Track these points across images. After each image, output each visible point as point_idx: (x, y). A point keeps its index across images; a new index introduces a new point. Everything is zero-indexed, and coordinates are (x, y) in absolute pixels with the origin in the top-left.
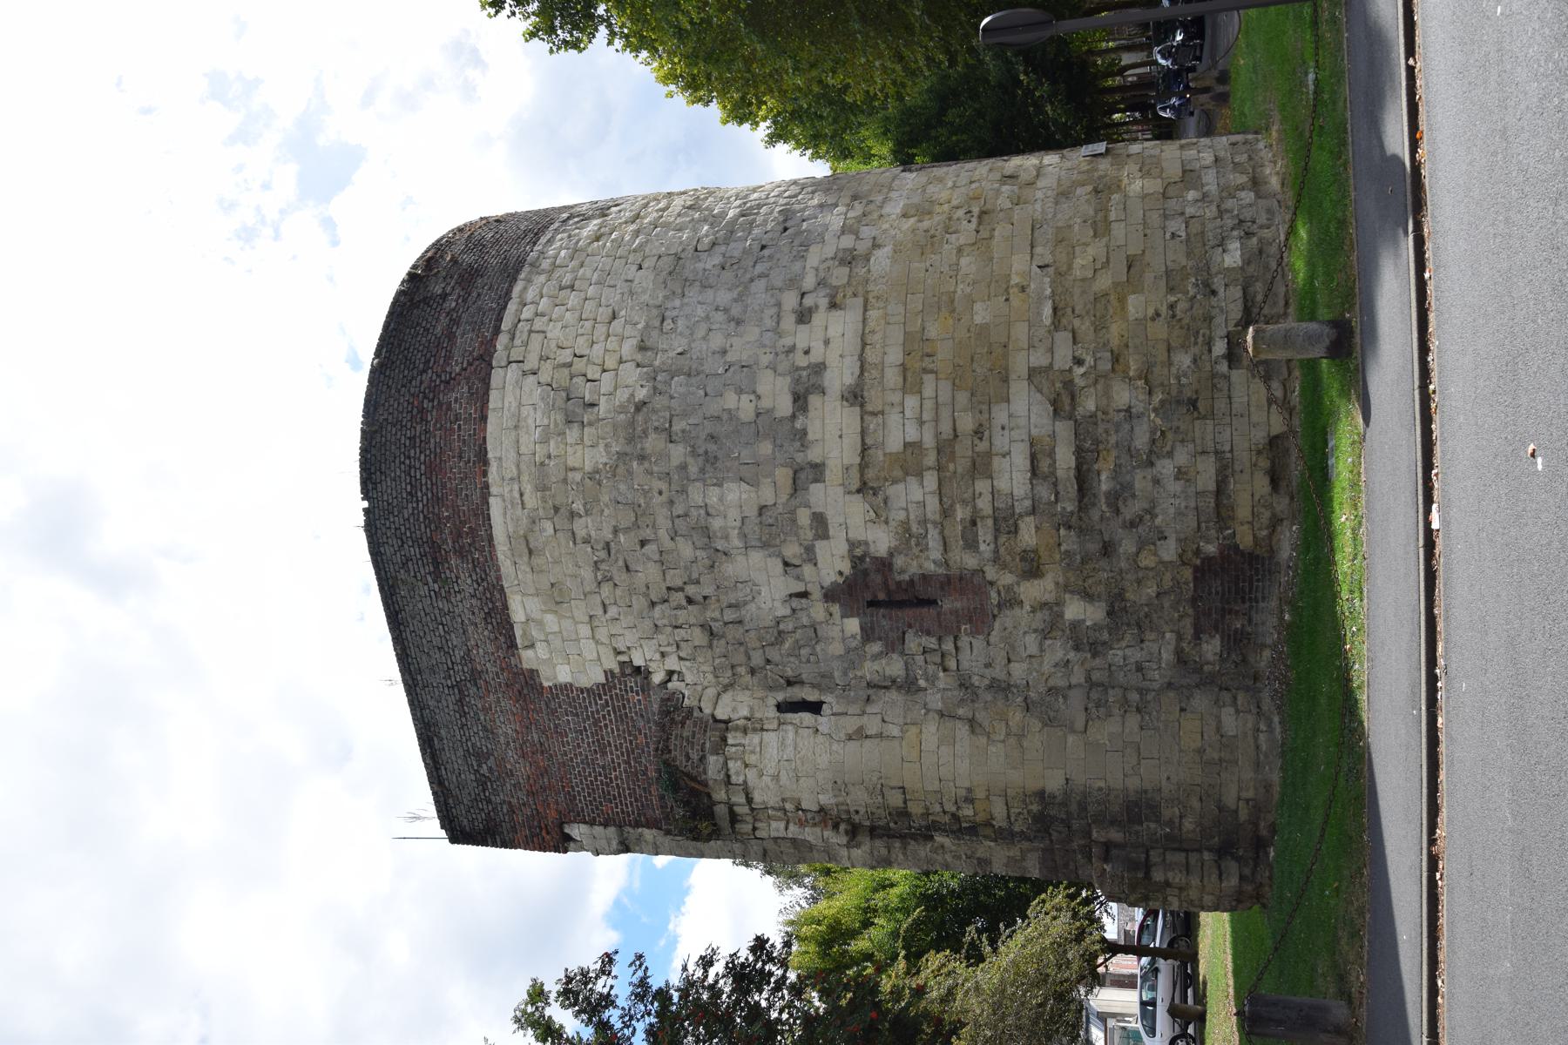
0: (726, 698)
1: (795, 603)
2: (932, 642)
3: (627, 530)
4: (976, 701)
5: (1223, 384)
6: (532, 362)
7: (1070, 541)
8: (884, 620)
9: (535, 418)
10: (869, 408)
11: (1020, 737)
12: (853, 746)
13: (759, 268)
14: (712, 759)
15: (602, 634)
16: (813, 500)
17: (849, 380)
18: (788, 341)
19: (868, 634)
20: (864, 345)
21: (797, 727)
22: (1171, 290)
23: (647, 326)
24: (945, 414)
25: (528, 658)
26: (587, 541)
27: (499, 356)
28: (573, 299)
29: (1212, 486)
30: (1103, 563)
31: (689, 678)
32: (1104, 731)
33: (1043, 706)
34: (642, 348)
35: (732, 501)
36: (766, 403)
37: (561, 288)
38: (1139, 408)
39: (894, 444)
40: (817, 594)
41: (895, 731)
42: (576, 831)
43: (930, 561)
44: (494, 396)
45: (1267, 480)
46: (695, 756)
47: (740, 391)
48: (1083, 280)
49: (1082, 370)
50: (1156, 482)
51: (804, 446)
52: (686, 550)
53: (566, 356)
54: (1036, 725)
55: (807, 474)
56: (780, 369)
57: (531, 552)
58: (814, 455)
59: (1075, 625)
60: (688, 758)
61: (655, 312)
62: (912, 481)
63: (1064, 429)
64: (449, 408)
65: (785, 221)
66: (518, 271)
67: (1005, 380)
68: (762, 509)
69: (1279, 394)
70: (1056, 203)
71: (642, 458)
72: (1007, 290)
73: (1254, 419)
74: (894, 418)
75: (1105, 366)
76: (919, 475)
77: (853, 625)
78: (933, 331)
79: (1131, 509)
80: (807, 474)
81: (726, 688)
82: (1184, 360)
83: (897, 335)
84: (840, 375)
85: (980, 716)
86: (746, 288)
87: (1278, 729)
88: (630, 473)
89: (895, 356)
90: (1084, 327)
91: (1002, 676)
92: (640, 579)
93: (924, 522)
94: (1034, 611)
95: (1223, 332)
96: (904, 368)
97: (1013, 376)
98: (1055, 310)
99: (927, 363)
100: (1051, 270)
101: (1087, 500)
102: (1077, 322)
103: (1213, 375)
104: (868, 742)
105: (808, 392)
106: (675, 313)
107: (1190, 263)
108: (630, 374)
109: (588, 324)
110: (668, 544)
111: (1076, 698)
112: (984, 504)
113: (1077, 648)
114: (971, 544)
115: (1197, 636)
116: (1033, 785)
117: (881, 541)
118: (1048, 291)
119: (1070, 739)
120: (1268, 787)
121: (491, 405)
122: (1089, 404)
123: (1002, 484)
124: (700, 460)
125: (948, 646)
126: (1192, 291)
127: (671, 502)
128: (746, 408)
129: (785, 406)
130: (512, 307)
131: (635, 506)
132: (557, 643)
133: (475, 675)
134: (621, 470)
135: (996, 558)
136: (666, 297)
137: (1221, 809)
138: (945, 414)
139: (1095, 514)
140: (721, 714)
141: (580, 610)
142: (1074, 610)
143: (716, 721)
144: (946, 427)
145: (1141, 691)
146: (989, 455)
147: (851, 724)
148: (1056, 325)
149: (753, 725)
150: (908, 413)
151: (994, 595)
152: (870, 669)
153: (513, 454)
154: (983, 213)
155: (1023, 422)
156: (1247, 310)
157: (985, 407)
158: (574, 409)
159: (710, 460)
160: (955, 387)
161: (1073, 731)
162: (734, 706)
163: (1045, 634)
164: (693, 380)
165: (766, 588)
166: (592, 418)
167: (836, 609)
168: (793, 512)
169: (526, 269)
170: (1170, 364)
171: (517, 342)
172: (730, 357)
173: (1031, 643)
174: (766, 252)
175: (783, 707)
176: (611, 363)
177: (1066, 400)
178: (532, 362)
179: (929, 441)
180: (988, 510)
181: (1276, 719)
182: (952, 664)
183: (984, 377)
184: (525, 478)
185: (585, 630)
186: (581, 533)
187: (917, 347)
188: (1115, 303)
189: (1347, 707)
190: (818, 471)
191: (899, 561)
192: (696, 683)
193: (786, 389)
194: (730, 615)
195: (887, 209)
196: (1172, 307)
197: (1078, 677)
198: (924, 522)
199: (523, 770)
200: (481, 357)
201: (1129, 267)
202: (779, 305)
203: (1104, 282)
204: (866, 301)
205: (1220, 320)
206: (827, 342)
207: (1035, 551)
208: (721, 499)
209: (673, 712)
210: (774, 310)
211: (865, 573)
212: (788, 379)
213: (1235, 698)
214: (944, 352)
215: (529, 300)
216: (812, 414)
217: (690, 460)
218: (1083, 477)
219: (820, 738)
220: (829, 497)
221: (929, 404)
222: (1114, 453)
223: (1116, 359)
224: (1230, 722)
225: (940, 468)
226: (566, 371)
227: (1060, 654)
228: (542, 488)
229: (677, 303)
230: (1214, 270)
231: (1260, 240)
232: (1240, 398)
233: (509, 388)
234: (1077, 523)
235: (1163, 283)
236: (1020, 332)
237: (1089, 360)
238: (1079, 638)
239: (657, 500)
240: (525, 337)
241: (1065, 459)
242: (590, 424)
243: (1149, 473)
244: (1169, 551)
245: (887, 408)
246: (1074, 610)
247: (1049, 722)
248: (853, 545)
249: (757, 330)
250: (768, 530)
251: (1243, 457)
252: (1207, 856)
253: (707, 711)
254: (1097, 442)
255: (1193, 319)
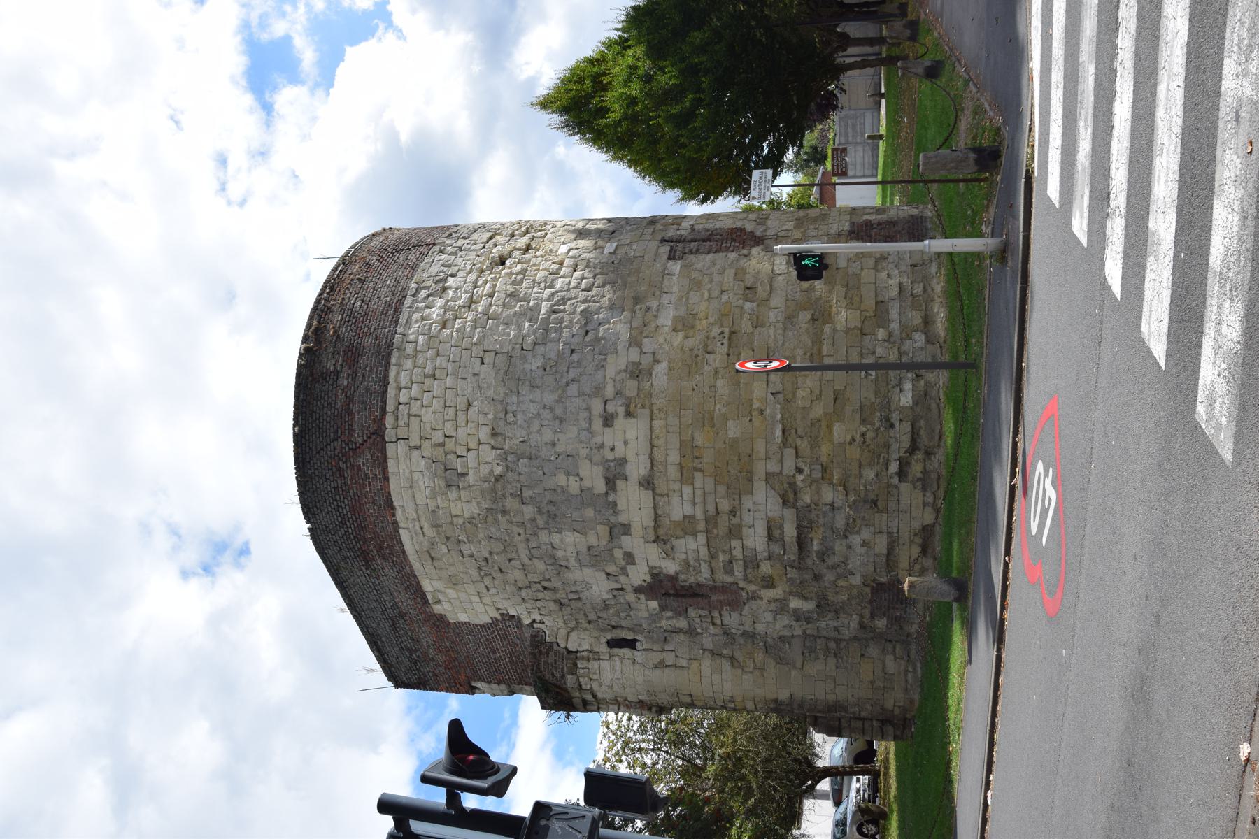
0: (574, 635)
1: (615, 593)
2: (705, 613)
3: (498, 554)
4: (730, 648)
5: (894, 492)
6: (415, 441)
7: (793, 573)
8: (673, 602)
9: (423, 481)
10: (658, 491)
11: (762, 669)
12: (658, 672)
13: (573, 373)
14: (569, 677)
15: (487, 600)
16: (623, 545)
17: (643, 471)
18: (598, 440)
19: (663, 608)
20: (652, 447)
21: (622, 659)
22: (863, 421)
23: (495, 417)
24: (710, 499)
25: (437, 609)
26: (472, 556)
27: (389, 433)
28: (437, 388)
29: (885, 551)
30: (814, 583)
31: (547, 623)
32: (814, 668)
33: (775, 649)
34: (494, 434)
35: (569, 543)
36: (587, 483)
37: (426, 376)
38: (838, 503)
39: (677, 515)
40: (629, 589)
41: (684, 663)
42: (479, 685)
43: (704, 576)
44: (391, 463)
45: (919, 550)
46: (558, 675)
47: (568, 474)
48: (804, 408)
49: (802, 477)
50: (849, 547)
51: (615, 513)
52: (540, 566)
53: (438, 437)
54: (771, 663)
55: (619, 530)
56: (595, 459)
57: (432, 559)
58: (622, 519)
59: (795, 610)
60: (553, 675)
61: (500, 407)
62: (690, 539)
63: (789, 514)
64: (359, 469)
65: (586, 324)
66: (389, 355)
67: (750, 480)
68: (589, 548)
69: (931, 500)
70: (785, 329)
71: (504, 512)
72: (750, 412)
73: (913, 514)
74: (675, 500)
75: (817, 475)
76: (694, 534)
77: (654, 604)
78: (700, 441)
79: (832, 561)
80: (619, 530)
81: (572, 630)
82: (870, 474)
83: (674, 441)
84: (637, 468)
85: (737, 655)
86: (564, 391)
87: (919, 671)
88: (497, 521)
89: (674, 457)
90: (803, 445)
91: (751, 630)
92: (510, 577)
93: (698, 560)
94: (769, 602)
95: (897, 457)
96: (681, 467)
97: (755, 478)
98: (784, 431)
99: (696, 464)
100: (781, 396)
101: (804, 553)
102: (799, 441)
103: (889, 485)
104: (667, 670)
105: (615, 478)
106: (514, 408)
107: (878, 401)
108: (489, 455)
109: (451, 411)
110: (527, 561)
111: (797, 644)
112: (737, 553)
113: (797, 620)
114: (730, 572)
115: (872, 617)
116: (772, 696)
117: (670, 567)
118: (779, 416)
119: (793, 673)
120: (912, 702)
121: (390, 470)
122: (806, 498)
123: (749, 543)
124: (545, 516)
125: (716, 614)
126: (877, 424)
127: (528, 540)
128: (573, 486)
129: (600, 487)
130: (391, 391)
131: (503, 542)
132: (458, 603)
133: (402, 615)
134: (490, 519)
135: (745, 578)
136: (506, 394)
137: (883, 709)
138: (710, 499)
139: (809, 562)
140: (572, 647)
141: (471, 589)
142: (795, 603)
143: (570, 652)
144: (711, 508)
145: (838, 641)
146: (740, 526)
147: (656, 657)
148: (785, 443)
149: (594, 656)
150: (685, 497)
151: (744, 594)
152: (665, 624)
153: (411, 505)
154: (732, 333)
155: (762, 508)
156: (914, 441)
157: (736, 497)
158: (452, 479)
159: (552, 516)
160: (716, 482)
161: (795, 667)
162: (579, 641)
163: (777, 613)
164: (534, 462)
165: (598, 587)
166: (466, 484)
167: (642, 597)
168: (611, 550)
169: (395, 354)
170: (861, 476)
171: (401, 423)
172: (559, 448)
173: (769, 616)
174: (575, 357)
175: (613, 644)
176: (472, 445)
177: (791, 496)
178: (415, 441)
179: (699, 514)
180: (740, 556)
181: (919, 665)
182: (718, 622)
183: (738, 480)
184: (423, 519)
185: (475, 599)
186: (466, 552)
187: (688, 450)
188: (824, 427)
189: (948, 781)
190: (626, 529)
191: (682, 577)
192: (553, 626)
193: (600, 475)
194: (572, 596)
195: (661, 321)
196: (863, 435)
197: (798, 632)
198: (698, 560)
199: (441, 658)
200: (375, 433)
201: (835, 399)
202: (589, 409)
203: (818, 411)
204: (652, 412)
205: (895, 447)
206: (626, 443)
207: (771, 577)
208: (561, 540)
209: (538, 639)
210: (586, 414)
211: (661, 581)
212: (601, 468)
213: (894, 648)
214: (708, 458)
215: (403, 384)
216: (619, 493)
217: (538, 516)
218: (802, 542)
219: (637, 666)
220: (634, 543)
221: (699, 493)
222: (822, 529)
223: (824, 470)
224: (891, 665)
225: (708, 532)
226: (441, 449)
227: (786, 622)
228: (436, 526)
229: (514, 399)
230: (893, 407)
231: (926, 384)
232: (905, 501)
233: (401, 459)
234: (800, 565)
235: (858, 416)
236: (760, 446)
237: (807, 470)
238: (797, 615)
239: (517, 538)
240: (406, 419)
241: (790, 531)
242: (464, 488)
243: (844, 542)
244: (856, 580)
245: (671, 493)
246: (795, 603)
247: (780, 661)
248: (651, 568)
249: (575, 429)
250: (595, 558)
251: (905, 536)
252: (875, 723)
253: (562, 645)
254: (811, 522)
255: (877, 445)
